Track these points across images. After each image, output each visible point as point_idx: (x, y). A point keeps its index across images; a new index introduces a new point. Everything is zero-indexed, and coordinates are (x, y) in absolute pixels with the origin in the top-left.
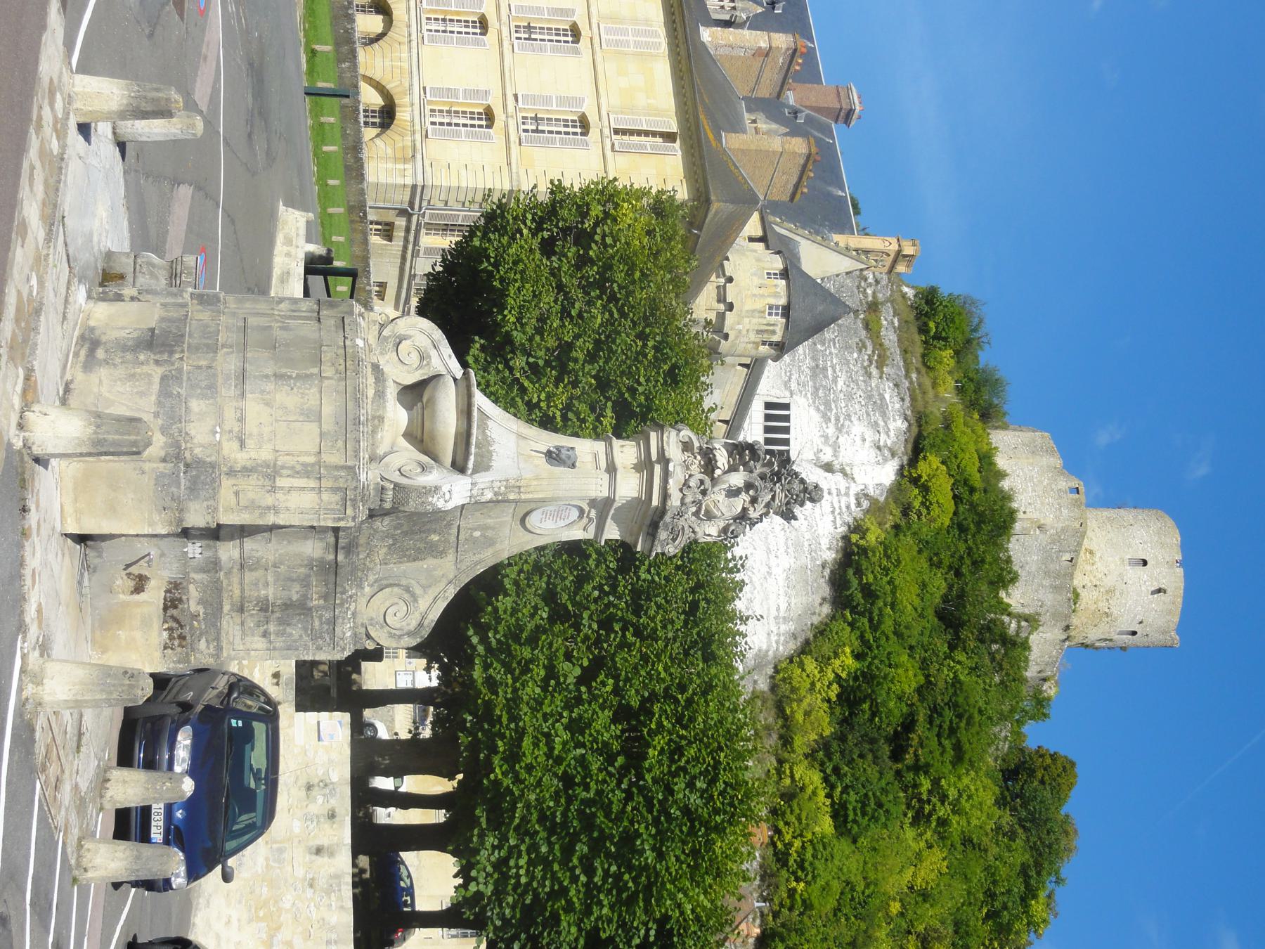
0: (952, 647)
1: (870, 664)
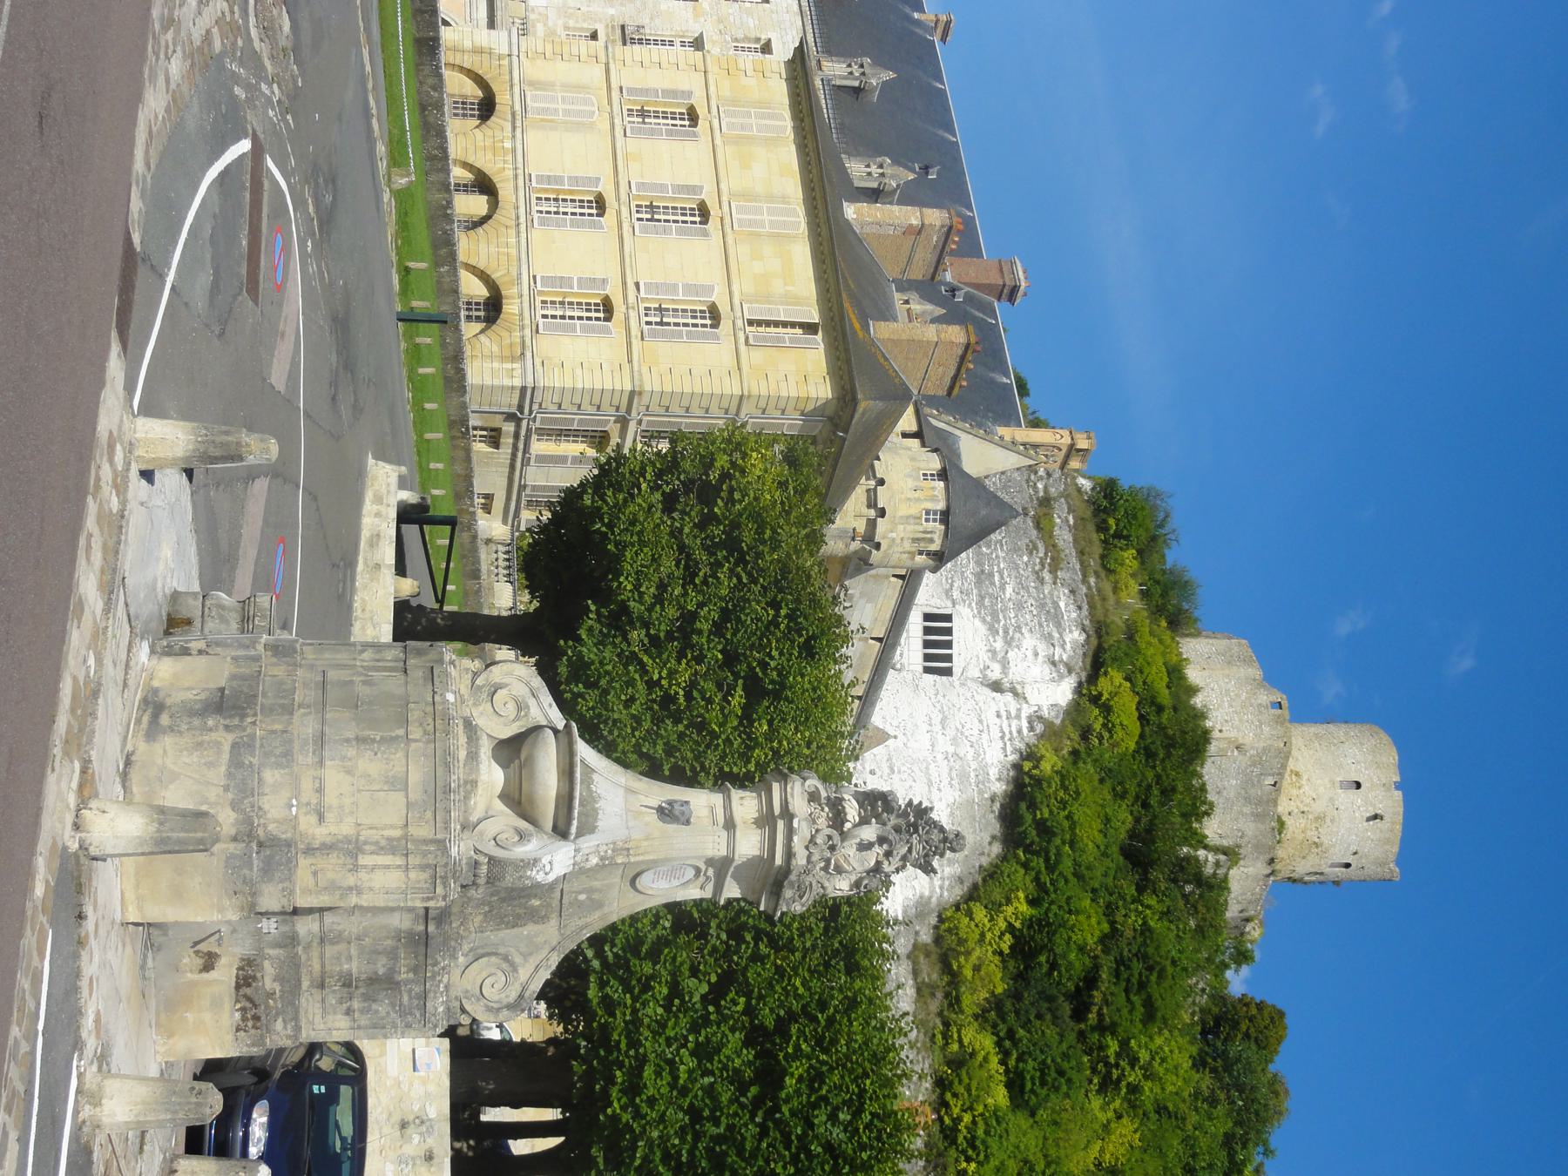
0: (1140, 889)
1: (1048, 909)
